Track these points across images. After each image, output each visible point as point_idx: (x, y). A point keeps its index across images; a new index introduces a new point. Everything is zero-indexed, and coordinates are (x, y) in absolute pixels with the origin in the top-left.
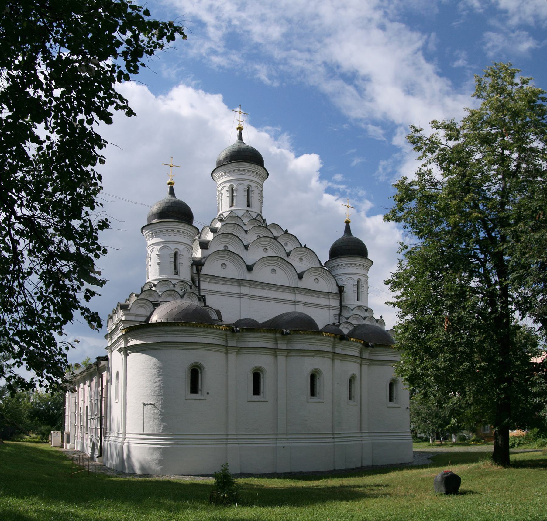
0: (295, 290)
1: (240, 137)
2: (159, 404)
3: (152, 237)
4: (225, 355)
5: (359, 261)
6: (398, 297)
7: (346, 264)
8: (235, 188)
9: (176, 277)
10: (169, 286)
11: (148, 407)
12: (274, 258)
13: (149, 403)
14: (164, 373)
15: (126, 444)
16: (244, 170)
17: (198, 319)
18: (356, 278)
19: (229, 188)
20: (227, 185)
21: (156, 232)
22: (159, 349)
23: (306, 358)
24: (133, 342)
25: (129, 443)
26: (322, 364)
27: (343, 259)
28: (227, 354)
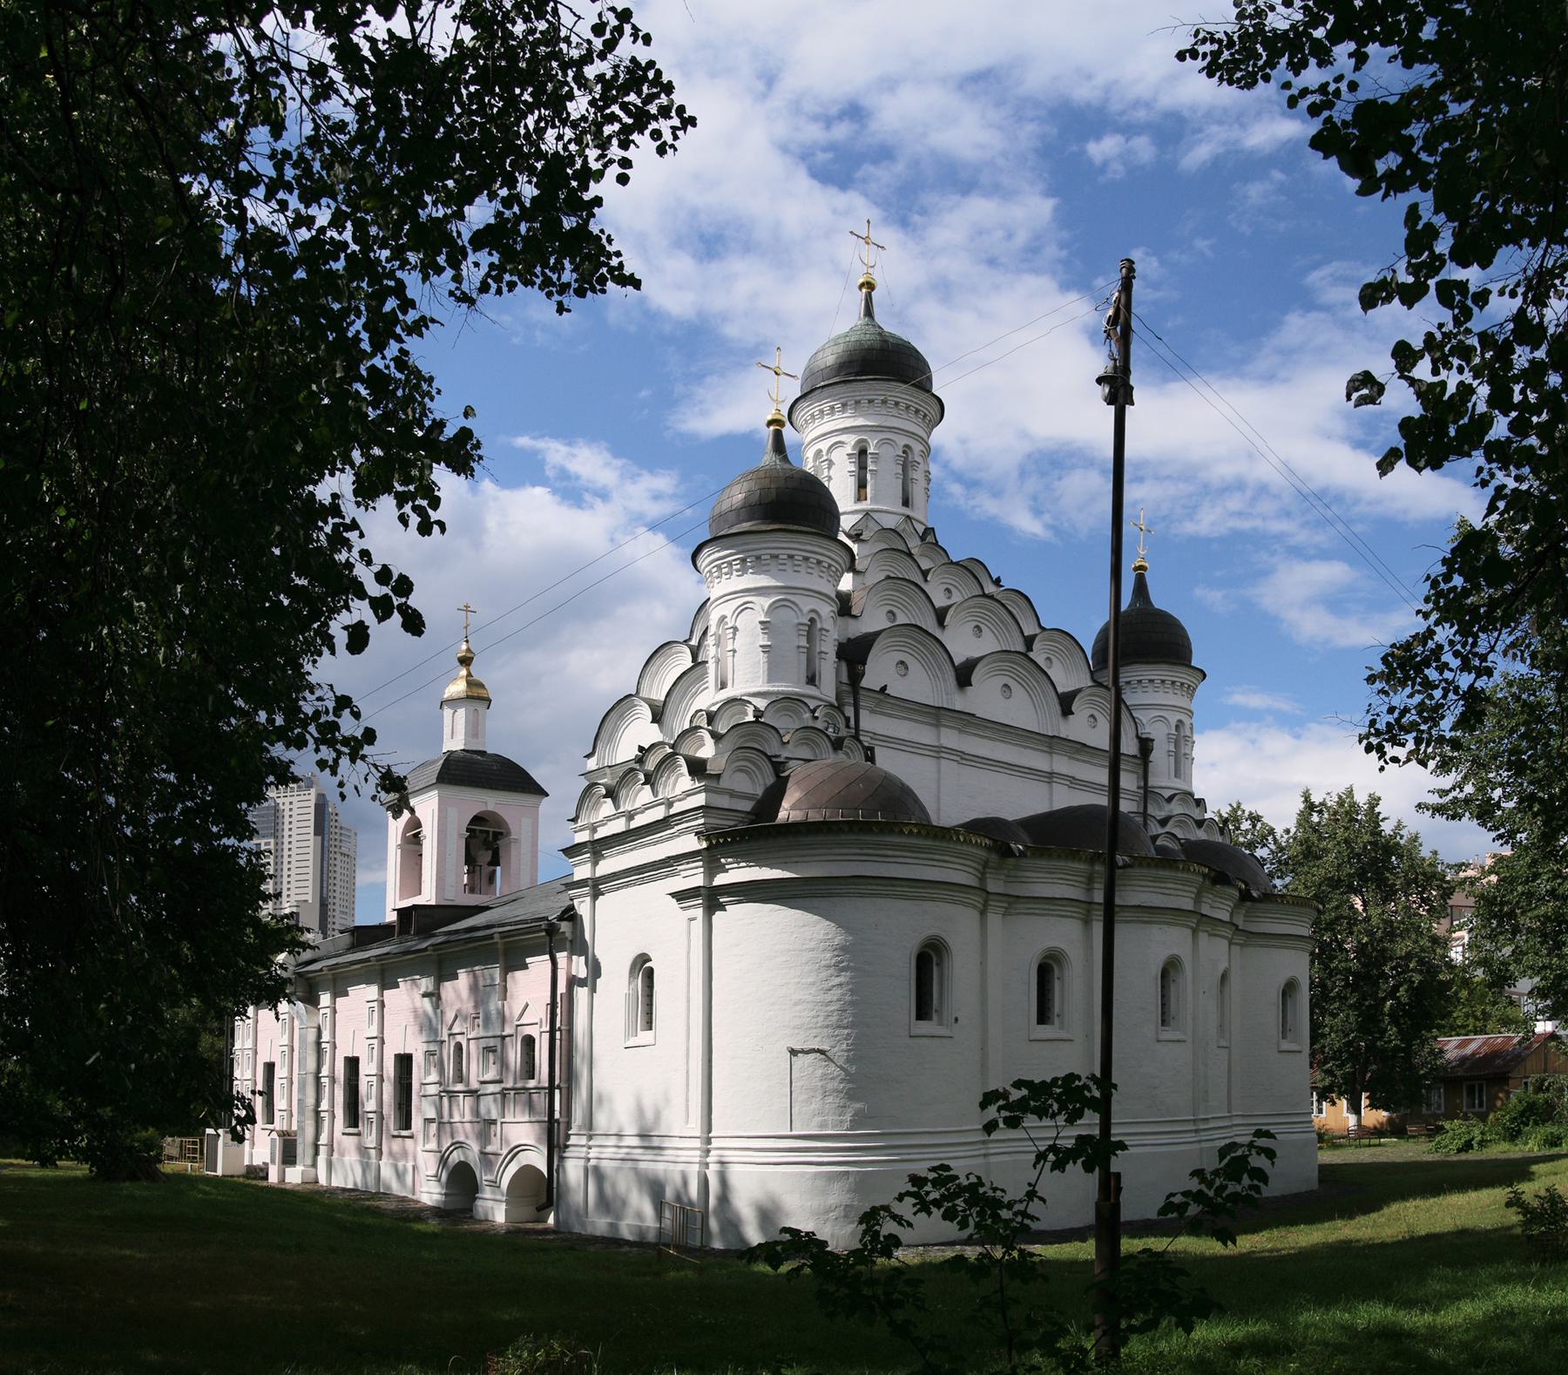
0: (1053, 743)
1: (869, 312)
2: (839, 1051)
3: (743, 571)
4: (975, 914)
5: (1180, 675)
6: (1443, 793)
7: (1151, 681)
8: (871, 450)
9: (811, 690)
10: (798, 714)
11: (801, 1060)
12: (1012, 656)
13: (806, 1047)
14: (853, 960)
15: (713, 1168)
16: (897, 404)
17: (884, 815)
18: (1173, 718)
19: (854, 447)
20: (851, 440)
21: (758, 558)
22: (839, 895)
23: (1155, 929)
24: (738, 873)
25: (722, 1163)
26: (957, 924)
27: (1144, 667)
28: (983, 913)
